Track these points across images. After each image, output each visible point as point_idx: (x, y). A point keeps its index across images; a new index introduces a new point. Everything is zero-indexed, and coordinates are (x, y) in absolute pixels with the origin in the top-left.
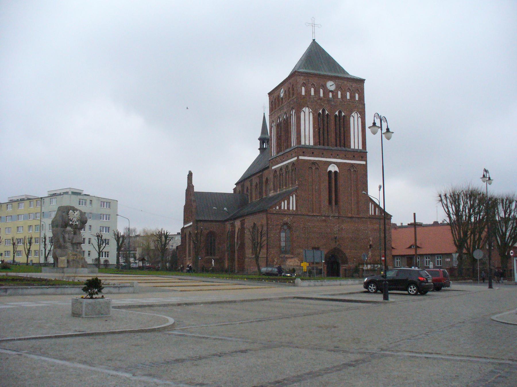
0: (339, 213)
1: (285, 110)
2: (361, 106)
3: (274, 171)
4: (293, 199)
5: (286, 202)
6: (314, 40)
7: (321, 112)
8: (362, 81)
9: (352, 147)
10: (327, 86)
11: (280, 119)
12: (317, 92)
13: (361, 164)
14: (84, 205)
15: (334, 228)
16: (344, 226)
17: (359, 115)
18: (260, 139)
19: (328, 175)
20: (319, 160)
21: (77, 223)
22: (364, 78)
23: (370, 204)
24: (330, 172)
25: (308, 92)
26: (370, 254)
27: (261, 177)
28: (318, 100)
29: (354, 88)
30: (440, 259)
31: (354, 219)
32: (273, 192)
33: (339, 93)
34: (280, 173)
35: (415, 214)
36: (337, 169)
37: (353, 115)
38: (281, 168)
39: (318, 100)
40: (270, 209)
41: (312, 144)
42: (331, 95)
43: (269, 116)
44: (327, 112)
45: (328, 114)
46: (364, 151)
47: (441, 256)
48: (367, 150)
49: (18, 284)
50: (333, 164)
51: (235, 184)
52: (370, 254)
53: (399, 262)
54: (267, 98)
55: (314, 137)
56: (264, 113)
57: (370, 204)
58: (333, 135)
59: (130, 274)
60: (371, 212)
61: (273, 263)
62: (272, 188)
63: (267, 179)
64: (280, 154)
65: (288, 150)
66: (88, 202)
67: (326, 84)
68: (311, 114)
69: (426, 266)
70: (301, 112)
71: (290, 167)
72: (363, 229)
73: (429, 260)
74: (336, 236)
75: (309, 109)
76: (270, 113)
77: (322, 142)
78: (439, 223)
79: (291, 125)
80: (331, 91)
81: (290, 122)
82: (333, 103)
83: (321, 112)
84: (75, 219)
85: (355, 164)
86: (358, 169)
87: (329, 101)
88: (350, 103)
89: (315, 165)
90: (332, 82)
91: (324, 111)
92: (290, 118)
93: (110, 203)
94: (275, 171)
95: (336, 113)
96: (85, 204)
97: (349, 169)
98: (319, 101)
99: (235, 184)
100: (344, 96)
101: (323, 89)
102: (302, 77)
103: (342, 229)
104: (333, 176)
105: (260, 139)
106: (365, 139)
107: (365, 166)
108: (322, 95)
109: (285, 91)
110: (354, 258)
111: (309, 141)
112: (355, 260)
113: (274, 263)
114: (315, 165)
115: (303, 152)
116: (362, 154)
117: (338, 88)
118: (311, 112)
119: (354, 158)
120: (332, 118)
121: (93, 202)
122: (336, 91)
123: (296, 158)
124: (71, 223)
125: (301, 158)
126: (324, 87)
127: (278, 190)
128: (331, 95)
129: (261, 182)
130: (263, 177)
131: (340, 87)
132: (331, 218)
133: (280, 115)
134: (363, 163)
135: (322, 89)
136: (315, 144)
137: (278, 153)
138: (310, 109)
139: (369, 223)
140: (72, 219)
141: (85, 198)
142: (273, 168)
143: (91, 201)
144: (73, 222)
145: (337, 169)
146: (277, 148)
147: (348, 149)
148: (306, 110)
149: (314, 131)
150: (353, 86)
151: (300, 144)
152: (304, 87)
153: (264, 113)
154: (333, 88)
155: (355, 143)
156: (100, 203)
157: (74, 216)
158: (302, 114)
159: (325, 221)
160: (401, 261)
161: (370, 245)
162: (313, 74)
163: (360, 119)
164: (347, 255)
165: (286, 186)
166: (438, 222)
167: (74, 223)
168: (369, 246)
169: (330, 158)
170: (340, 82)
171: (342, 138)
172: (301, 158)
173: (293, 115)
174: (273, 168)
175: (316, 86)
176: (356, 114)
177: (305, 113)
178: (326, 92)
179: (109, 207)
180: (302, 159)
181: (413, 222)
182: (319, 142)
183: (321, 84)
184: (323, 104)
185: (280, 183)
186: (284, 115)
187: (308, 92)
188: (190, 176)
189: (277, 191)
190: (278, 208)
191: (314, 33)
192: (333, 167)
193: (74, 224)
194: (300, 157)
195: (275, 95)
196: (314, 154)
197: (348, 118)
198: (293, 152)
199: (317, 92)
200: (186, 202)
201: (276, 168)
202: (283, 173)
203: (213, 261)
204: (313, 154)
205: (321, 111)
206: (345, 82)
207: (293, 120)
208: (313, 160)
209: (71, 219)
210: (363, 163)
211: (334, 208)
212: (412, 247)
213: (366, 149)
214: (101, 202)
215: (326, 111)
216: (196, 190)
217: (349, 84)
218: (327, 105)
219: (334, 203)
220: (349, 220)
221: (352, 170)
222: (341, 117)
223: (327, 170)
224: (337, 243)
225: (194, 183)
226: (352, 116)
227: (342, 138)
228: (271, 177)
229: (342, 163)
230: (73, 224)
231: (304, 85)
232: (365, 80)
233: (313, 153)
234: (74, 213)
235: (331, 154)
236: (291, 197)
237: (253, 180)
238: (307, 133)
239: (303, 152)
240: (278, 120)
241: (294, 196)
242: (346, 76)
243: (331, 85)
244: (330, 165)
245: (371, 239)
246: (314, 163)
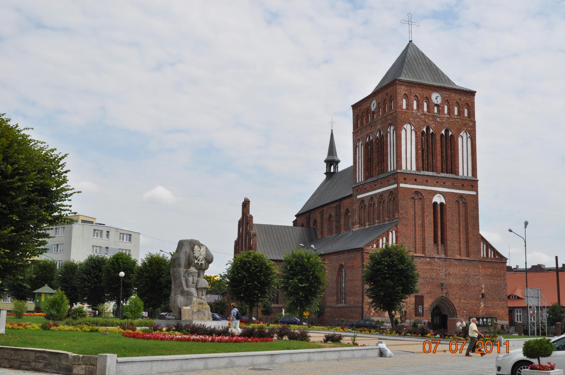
0: (446, 254)
1: (379, 127)
2: (471, 124)
3: (361, 200)
4: (392, 236)
5: (384, 239)
6: (411, 41)
7: (444, 133)
8: (472, 93)
10: (432, 99)
11: (369, 137)
13: (471, 195)
14: (99, 238)
15: (441, 272)
16: (452, 270)
17: (469, 135)
18: (326, 161)
19: (432, 208)
20: (423, 188)
21: (203, 262)
22: (473, 89)
23: (482, 244)
24: (435, 203)
25: (409, 105)
26: (482, 305)
27: (338, 208)
28: (422, 115)
29: (462, 101)
30: (520, 314)
31: (463, 262)
32: (359, 227)
33: (446, 107)
34: (370, 204)
35: (557, 257)
36: (443, 201)
37: (462, 135)
38: (372, 197)
39: (422, 115)
40: (367, 248)
41: (414, 168)
43: (353, 133)
44: (431, 131)
46: (474, 179)
47: (521, 310)
49: (323, 329)
50: (439, 193)
51: (295, 216)
52: (482, 305)
53: (520, 315)
54: (351, 112)
55: (417, 160)
56: (332, 130)
57: (482, 244)
58: (439, 158)
60: (483, 254)
61: (370, 313)
62: (358, 221)
63: (347, 211)
64: (369, 180)
65: (382, 176)
66: (105, 233)
68: (413, 132)
69: (517, 321)
70: (402, 130)
71: (386, 197)
72: (474, 274)
73: (520, 314)
74: (442, 282)
76: (354, 130)
77: (425, 166)
78: (513, 268)
79: (388, 145)
80: (437, 105)
81: (387, 141)
82: (438, 120)
83: (444, 133)
84: (201, 257)
85: (464, 194)
86: (467, 201)
87: (434, 117)
88: (458, 120)
89: (418, 194)
90: (438, 94)
91: (428, 129)
92: (387, 137)
93: (130, 235)
94: (362, 200)
95: (442, 132)
96: (101, 237)
97: (457, 201)
98: (423, 117)
99: (295, 216)
101: (468, 108)
102: (403, 87)
103: (449, 273)
104: (439, 209)
105: (326, 161)
106: (476, 165)
107: (476, 197)
108: (425, 109)
109: (379, 103)
110: (464, 309)
111: (411, 165)
112: (465, 312)
113: (371, 314)
114: (418, 194)
115: (405, 179)
116: (472, 184)
117: (446, 101)
118: (414, 129)
119: (463, 187)
120: (438, 138)
121: (111, 233)
122: (442, 105)
123: (395, 186)
124: (196, 261)
125: (402, 185)
126: (428, 100)
127: (367, 224)
129: (338, 215)
130: (342, 207)
131: (447, 100)
132: (436, 260)
133: (370, 133)
134: (474, 193)
135: (425, 101)
136: (418, 169)
137: (366, 178)
139: (480, 267)
140: (198, 257)
141: (101, 228)
142: (359, 197)
143: (108, 232)
144: (198, 261)
145: (443, 201)
146: (365, 173)
148: (408, 127)
149: (417, 153)
150: (462, 99)
151: (401, 169)
152: (406, 99)
153: (332, 130)
154: (439, 101)
155: (464, 170)
156: (119, 235)
157: (200, 253)
158: (403, 132)
159: (429, 263)
160: (523, 315)
161: (483, 294)
162: (416, 84)
163: (469, 140)
164: (455, 306)
165: (378, 218)
166: (511, 267)
167: (200, 262)
168: (481, 296)
169: (435, 186)
170: (448, 94)
171: (449, 163)
172: (402, 185)
173: (390, 133)
174: (359, 197)
175: (419, 98)
176: (465, 133)
177: (406, 131)
179: (130, 241)
180: (403, 187)
181: (555, 266)
182: (423, 167)
183: (425, 96)
184: (427, 120)
185: (369, 216)
186: (377, 133)
187: (409, 105)
188: (246, 204)
189: (365, 226)
190: (375, 246)
191: (410, 33)
192: (439, 197)
193: (200, 263)
194: (401, 184)
195: (364, 107)
196: (417, 181)
198: (391, 177)
199: (420, 106)
200: (238, 236)
201: (363, 197)
202: (374, 204)
203: (284, 311)
204: (416, 182)
205: (424, 129)
206: (453, 95)
207: (391, 139)
208: (416, 189)
209: (197, 257)
210: (474, 193)
211: (440, 247)
212: (511, 298)
213: (476, 177)
214: (121, 234)
215: (431, 129)
216: (255, 221)
217: (457, 97)
218: (433, 122)
219: (440, 242)
220: (456, 263)
221: (461, 202)
222: (448, 137)
223: (432, 201)
224: (444, 291)
225: (252, 212)
226: (461, 136)
227: (449, 163)
228: (356, 206)
229: (449, 192)
230: (198, 263)
231: (406, 96)
232: (475, 92)
233: (416, 180)
234: (201, 249)
235: (437, 182)
236: (390, 233)
237: (325, 212)
238: (409, 156)
239: (405, 179)
240: (366, 139)
241: (394, 232)
242: (454, 87)
243: (436, 98)
244: (434, 195)
245: (483, 286)
246: (417, 192)
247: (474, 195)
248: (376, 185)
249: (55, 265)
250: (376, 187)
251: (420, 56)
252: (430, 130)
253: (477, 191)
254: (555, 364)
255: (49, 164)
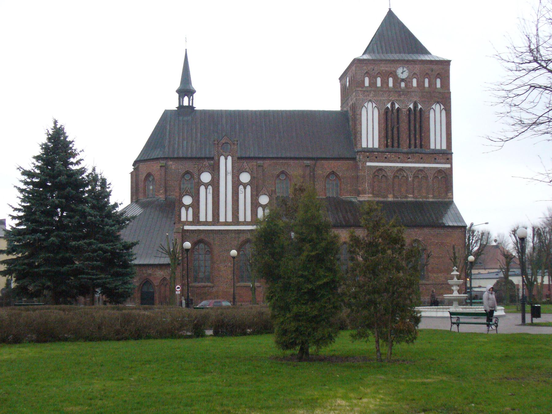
6: (390, 9)
7: (412, 108)
9: (432, 147)
12: (385, 82)
22: (449, 59)
41: (376, 145)
42: (403, 85)
45: (421, 108)
46: (448, 152)
48: (453, 151)
59: (178, 213)
67: (395, 72)
71: (390, 174)
75: (372, 104)
80: (403, 80)
83: (412, 108)
100: (421, 84)
107: (451, 169)
119: (435, 161)
128: (403, 85)
138: (374, 103)
147: (423, 150)
154: (405, 76)
163: (444, 113)
178: (397, 81)
197: (512, 114)
199: (385, 82)
204: (376, 159)
210: (448, 166)
213: (451, 149)
226: (432, 108)
232: (450, 61)
247: (447, 169)
248: (409, 158)
249: (110, 203)
250: (409, 160)
251: (394, 26)
252: (395, 105)
253: (451, 163)
254: (56, 122)
255: (51, 155)
